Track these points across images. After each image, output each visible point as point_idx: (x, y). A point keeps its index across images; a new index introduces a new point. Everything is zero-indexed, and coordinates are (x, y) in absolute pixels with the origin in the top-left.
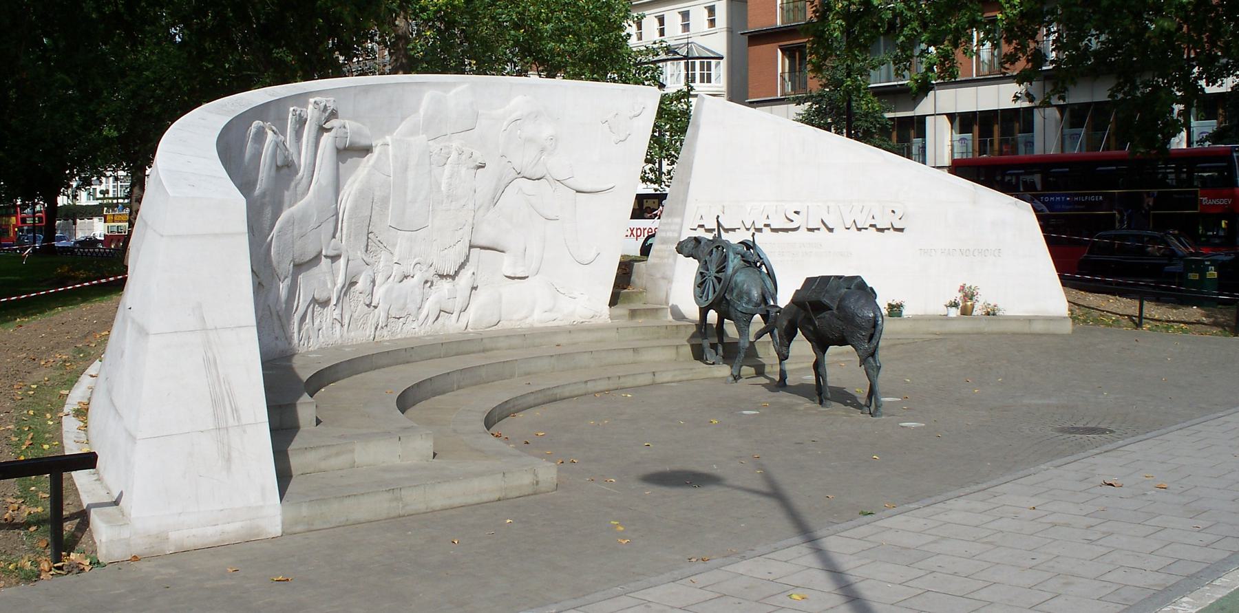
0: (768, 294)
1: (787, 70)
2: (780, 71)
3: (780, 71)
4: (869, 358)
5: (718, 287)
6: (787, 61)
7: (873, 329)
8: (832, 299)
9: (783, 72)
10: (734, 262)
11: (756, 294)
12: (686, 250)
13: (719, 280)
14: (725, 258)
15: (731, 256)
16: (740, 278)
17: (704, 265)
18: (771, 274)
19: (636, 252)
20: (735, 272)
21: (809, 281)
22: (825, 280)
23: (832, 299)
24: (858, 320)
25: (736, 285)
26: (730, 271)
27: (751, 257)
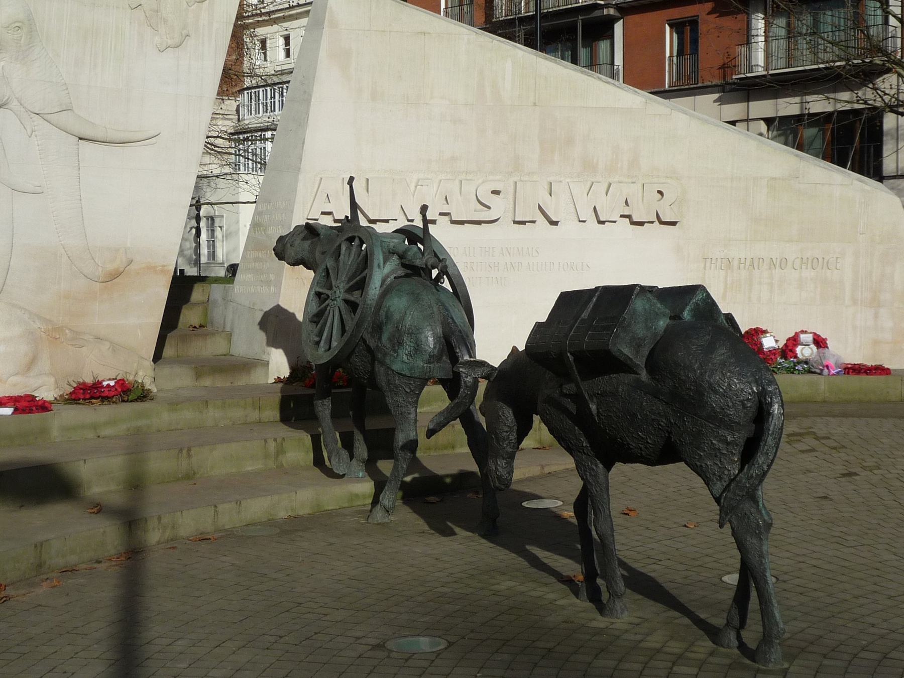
0: (456, 339)
1: (675, 54)
2: (668, 54)
3: (668, 54)
4: (738, 507)
5: (349, 326)
6: (675, 36)
7: (756, 434)
8: (637, 345)
9: (671, 56)
10: (383, 272)
11: (430, 340)
12: (291, 252)
13: (353, 306)
14: (365, 262)
15: (378, 257)
16: (398, 304)
17: (325, 280)
18: (461, 295)
19: (446, 218)
20: (386, 292)
21: (568, 302)
22: (616, 299)
23: (637, 345)
24: (714, 400)
25: (388, 316)
26: (374, 288)
27: (419, 258)
